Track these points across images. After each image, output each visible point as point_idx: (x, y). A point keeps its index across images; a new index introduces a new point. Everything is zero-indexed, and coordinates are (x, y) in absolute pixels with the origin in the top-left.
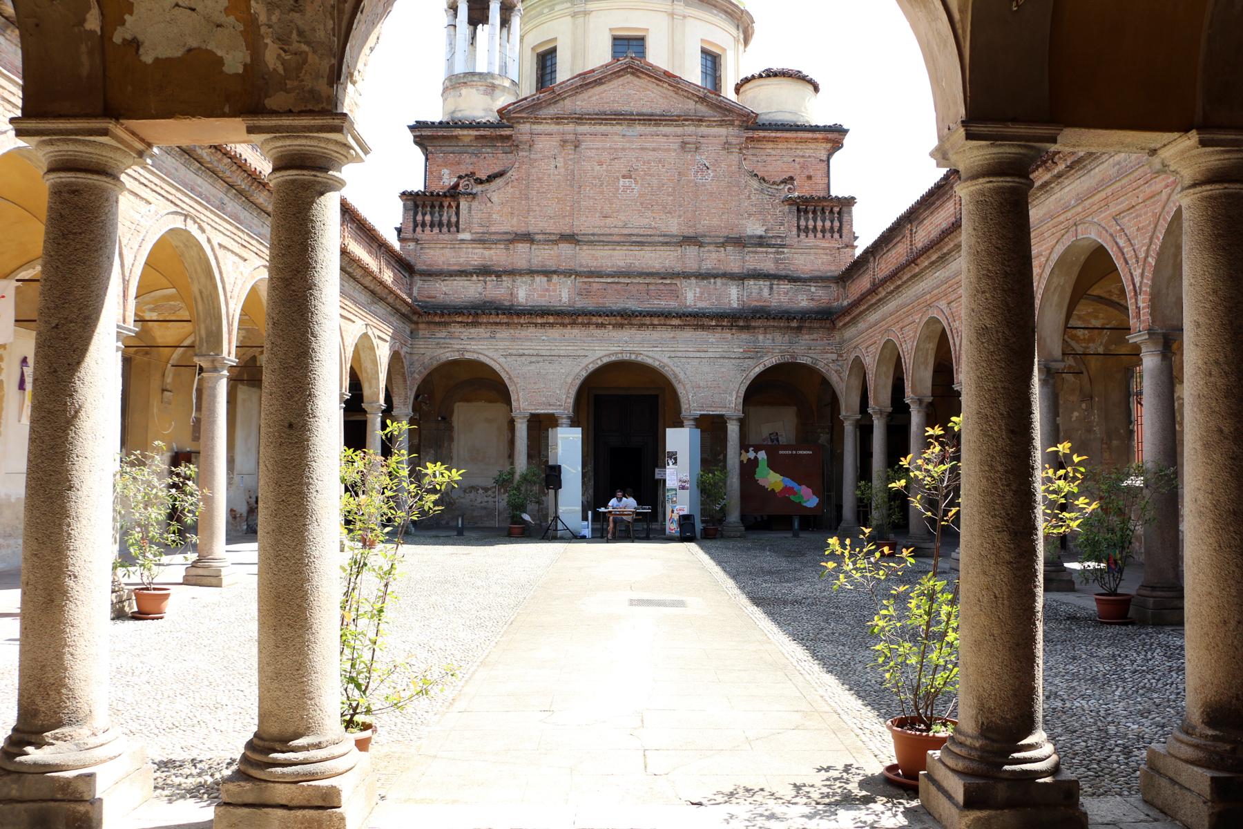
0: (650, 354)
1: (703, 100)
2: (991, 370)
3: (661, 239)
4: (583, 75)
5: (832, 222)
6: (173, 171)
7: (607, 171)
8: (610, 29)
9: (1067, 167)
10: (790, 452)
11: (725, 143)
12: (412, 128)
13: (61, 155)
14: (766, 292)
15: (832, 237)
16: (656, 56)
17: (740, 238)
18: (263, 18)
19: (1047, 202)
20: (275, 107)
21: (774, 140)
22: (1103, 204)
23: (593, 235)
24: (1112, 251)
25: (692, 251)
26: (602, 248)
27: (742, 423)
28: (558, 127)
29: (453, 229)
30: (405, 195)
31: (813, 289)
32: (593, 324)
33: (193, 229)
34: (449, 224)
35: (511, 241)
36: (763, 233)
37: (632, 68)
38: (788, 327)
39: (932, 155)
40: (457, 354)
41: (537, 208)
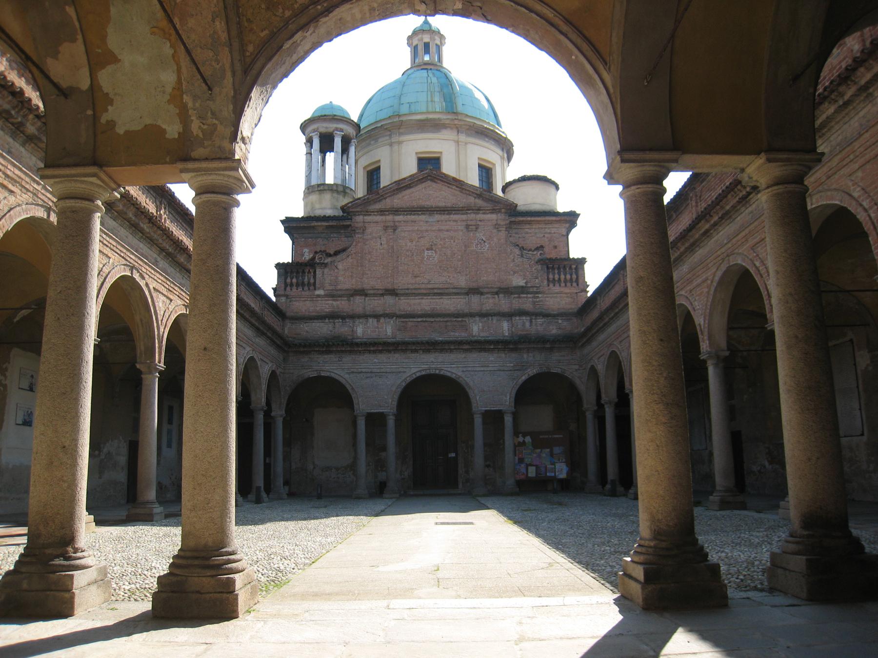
0: (449, 369)
1: (479, 196)
2: (646, 302)
3: (454, 291)
4: (398, 182)
5: (571, 275)
6: (125, 238)
7: (416, 246)
8: (416, 153)
9: (719, 218)
10: (547, 436)
11: (496, 225)
12: (283, 222)
13: (67, 190)
14: (527, 324)
15: (572, 285)
16: (448, 168)
17: (508, 288)
18: (190, 105)
19: (709, 243)
20: (197, 157)
21: (530, 223)
22: (744, 240)
23: (408, 289)
24: (752, 271)
25: (475, 299)
26: (414, 298)
27: (515, 416)
28: (382, 217)
29: (312, 288)
30: (279, 266)
31: (560, 321)
32: (409, 350)
33: (136, 276)
34: (309, 284)
35: (352, 295)
36: (524, 285)
37: (431, 176)
38: (543, 348)
39: (605, 177)
40: (316, 373)
41: (369, 273)
